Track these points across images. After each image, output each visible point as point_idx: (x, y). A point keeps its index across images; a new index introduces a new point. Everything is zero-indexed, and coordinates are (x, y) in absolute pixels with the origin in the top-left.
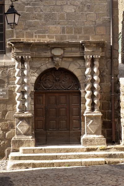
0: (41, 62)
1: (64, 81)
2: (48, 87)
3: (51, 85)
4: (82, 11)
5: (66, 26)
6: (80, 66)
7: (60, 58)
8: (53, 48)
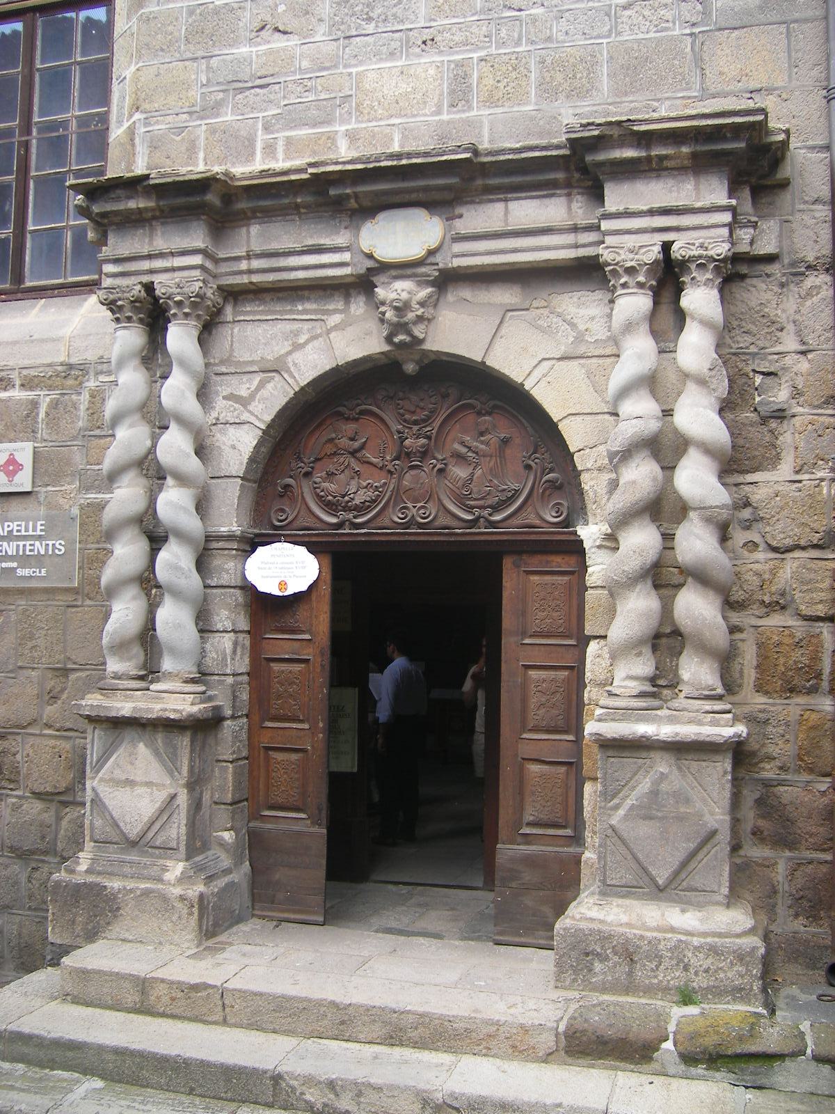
1: (460, 458)
2: (346, 509)
3: (371, 494)
5: (482, 53)
7: (422, 283)
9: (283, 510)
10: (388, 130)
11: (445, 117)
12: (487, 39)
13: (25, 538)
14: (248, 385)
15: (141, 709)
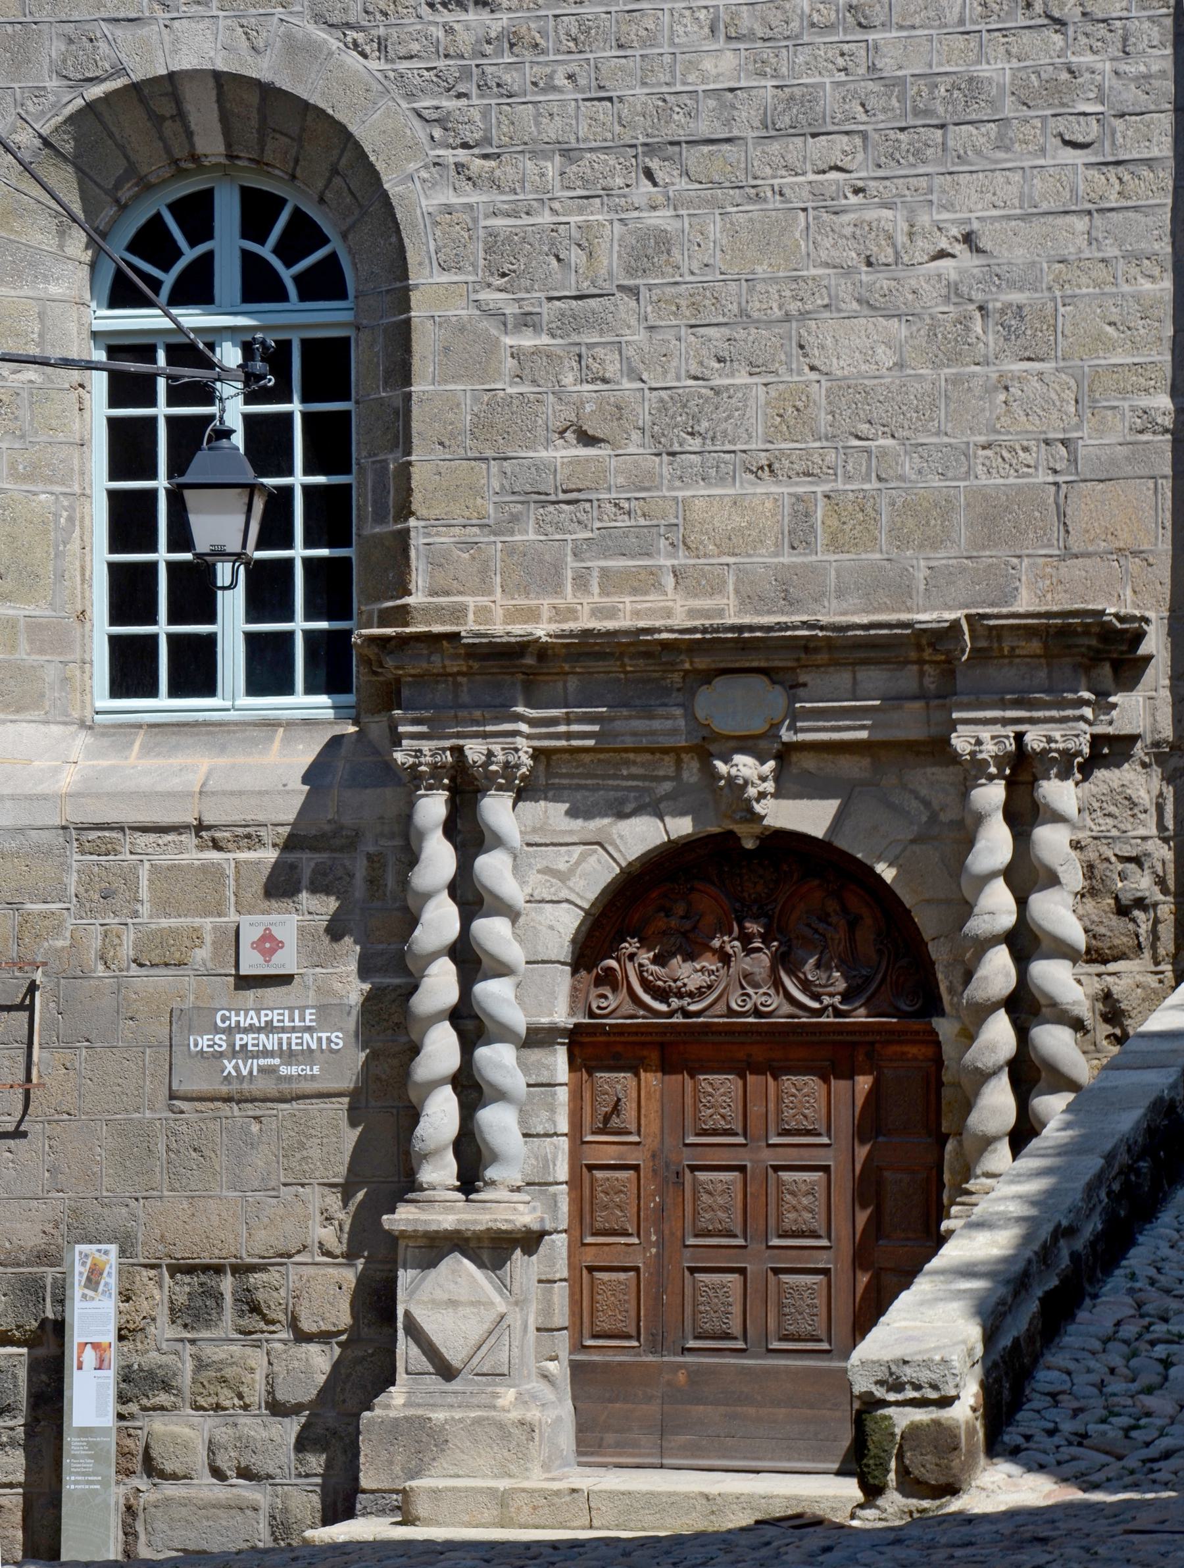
0: (616, 788)
2: (680, 996)
4: (955, 358)
5: (826, 487)
6: (933, 818)
8: (708, 677)
9: (605, 997)
10: (718, 570)
11: (785, 560)
12: (831, 471)
13: (294, 1029)
14: (566, 858)
15: (466, 1222)
